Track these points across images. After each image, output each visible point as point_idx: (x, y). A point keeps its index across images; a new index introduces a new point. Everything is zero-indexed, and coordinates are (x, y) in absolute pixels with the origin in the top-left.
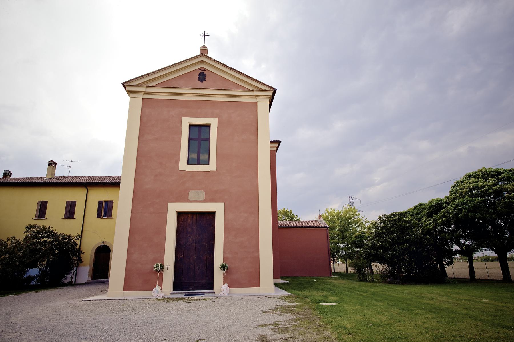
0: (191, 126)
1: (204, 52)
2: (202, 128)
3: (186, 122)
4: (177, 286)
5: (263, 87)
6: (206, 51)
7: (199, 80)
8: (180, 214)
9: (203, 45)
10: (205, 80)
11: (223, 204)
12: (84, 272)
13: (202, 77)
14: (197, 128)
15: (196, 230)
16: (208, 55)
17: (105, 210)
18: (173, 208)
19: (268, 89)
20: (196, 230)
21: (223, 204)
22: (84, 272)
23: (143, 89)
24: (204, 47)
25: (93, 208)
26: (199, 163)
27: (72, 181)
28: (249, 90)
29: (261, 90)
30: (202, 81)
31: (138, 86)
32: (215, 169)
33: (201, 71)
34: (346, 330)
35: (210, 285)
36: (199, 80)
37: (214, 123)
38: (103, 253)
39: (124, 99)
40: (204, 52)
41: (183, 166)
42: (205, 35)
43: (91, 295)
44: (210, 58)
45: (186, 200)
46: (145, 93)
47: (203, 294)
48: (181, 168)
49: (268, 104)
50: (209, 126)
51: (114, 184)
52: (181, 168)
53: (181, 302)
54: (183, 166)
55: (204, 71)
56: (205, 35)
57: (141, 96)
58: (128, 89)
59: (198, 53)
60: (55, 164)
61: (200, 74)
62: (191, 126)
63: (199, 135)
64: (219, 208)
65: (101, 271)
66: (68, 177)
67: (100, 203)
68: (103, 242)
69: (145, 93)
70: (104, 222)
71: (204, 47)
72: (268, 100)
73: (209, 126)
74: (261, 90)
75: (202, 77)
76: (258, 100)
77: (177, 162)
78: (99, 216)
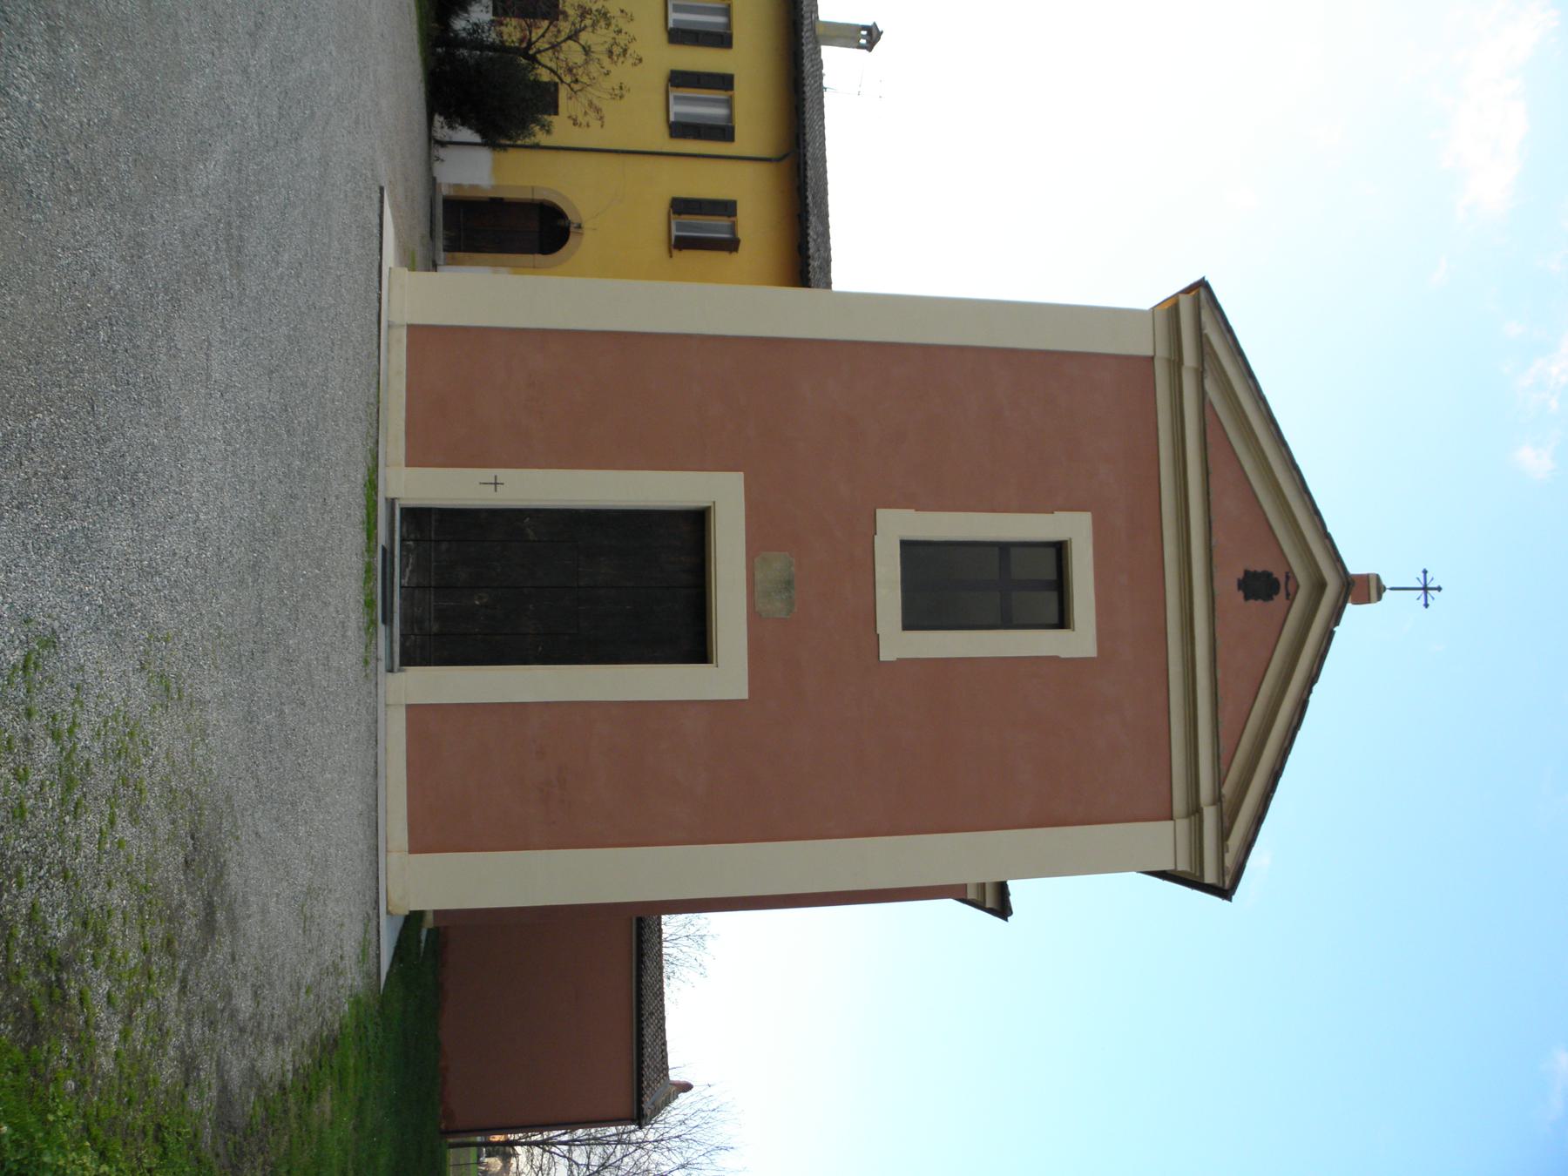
0: (1060, 550)
1: (1365, 589)
3: (1073, 528)
4: (421, 522)
5: (1235, 841)
6: (1365, 599)
7: (1247, 573)
8: (697, 521)
9: (1386, 582)
10: (1247, 598)
12: (474, 169)
13: (1259, 586)
14: (1051, 575)
15: (637, 587)
16: (1349, 606)
17: (699, 229)
18: (723, 495)
19: (1229, 860)
20: (637, 587)
22: (474, 169)
24: (1381, 590)
25: (706, 182)
26: (1060, 585)
27: (808, 105)
28: (1219, 781)
29: (1224, 834)
32: (888, 653)
33: (1282, 580)
35: (422, 648)
36: (1247, 573)
37: (1079, 640)
38: (537, 230)
39: (1143, 287)
40: (1365, 589)
41: (897, 525)
42: (1425, 589)
43: (394, 206)
44: (1336, 616)
45: (757, 543)
46: (1176, 363)
47: (387, 620)
48: (883, 515)
49: (1168, 866)
50: (1062, 621)
51: (802, 257)
52: (883, 515)
53: (361, 539)
54: (897, 525)
57: (1162, 352)
58: (1183, 298)
59: (1354, 567)
60: (870, 47)
61: (1267, 576)
62: (1060, 550)
63: (948, 585)
64: (725, 676)
65: (479, 228)
66: (820, 89)
67: (726, 208)
68: (579, 227)
69: (1176, 363)
70: (655, 223)
71: (1381, 590)
72: (1183, 866)
73: (1062, 621)
74: (1224, 834)
75: (1259, 586)
76: (1182, 825)
78: (681, 206)
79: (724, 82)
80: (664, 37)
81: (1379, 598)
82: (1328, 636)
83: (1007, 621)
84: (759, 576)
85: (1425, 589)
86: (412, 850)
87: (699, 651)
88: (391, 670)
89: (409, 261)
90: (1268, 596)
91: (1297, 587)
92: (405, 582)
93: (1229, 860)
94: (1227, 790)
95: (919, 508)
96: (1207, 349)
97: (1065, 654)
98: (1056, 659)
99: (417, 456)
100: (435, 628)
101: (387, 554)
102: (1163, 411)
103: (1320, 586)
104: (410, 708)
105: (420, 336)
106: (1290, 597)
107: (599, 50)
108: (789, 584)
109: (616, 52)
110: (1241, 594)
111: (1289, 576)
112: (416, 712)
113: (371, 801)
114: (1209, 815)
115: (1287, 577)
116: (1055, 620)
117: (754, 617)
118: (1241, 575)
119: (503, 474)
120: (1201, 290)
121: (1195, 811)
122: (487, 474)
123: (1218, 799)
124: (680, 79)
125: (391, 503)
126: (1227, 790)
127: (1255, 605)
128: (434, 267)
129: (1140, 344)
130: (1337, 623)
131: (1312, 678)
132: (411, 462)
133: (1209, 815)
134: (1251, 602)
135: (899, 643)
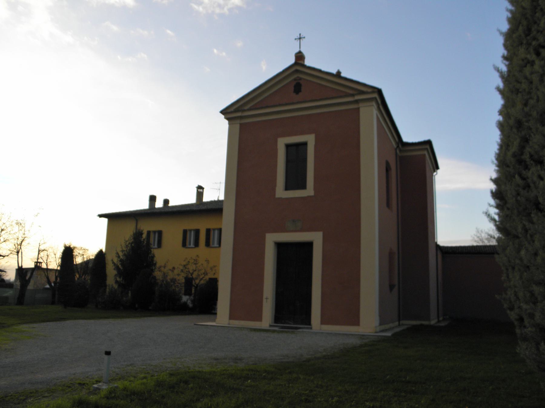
1: (300, 57)
3: (282, 143)
9: (297, 50)
13: (298, 88)
18: (271, 239)
19: (370, 90)
20: (294, 261)
24: (300, 52)
29: (363, 93)
31: (236, 111)
35: (307, 320)
37: (310, 139)
40: (300, 57)
41: (281, 192)
42: (300, 38)
46: (241, 118)
54: (281, 192)
57: (238, 121)
61: (295, 86)
64: (316, 238)
74: (363, 93)
75: (298, 88)
76: (361, 105)
79: (208, 231)
80: (197, 248)
85: (300, 38)
87: (309, 246)
88: (311, 328)
89: (214, 320)
91: (298, 77)
93: (370, 90)
95: (275, 186)
97: (314, 143)
99: (259, 318)
101: (282, 327)
102: (252, 120)
103: (297, 71)
105: (232, 317)
106: (301, 79)
107: (194, 267)
109: (196, 262)
111: (295, 80)
112: (323, 322)
114: (252, 104)
117: (302, 230)
119: (265, 297)
120: (223, 112)
121: (357, 102)
122: (264, 300)
123: (353, 95)
124: (208, 244)
125: (271, 326)
126: (351, 92)
127: (303, 89)
128: (216, 314)
129: (237, 127)
131: (320, 71)
133: (252, 104)
135: (309, 191)
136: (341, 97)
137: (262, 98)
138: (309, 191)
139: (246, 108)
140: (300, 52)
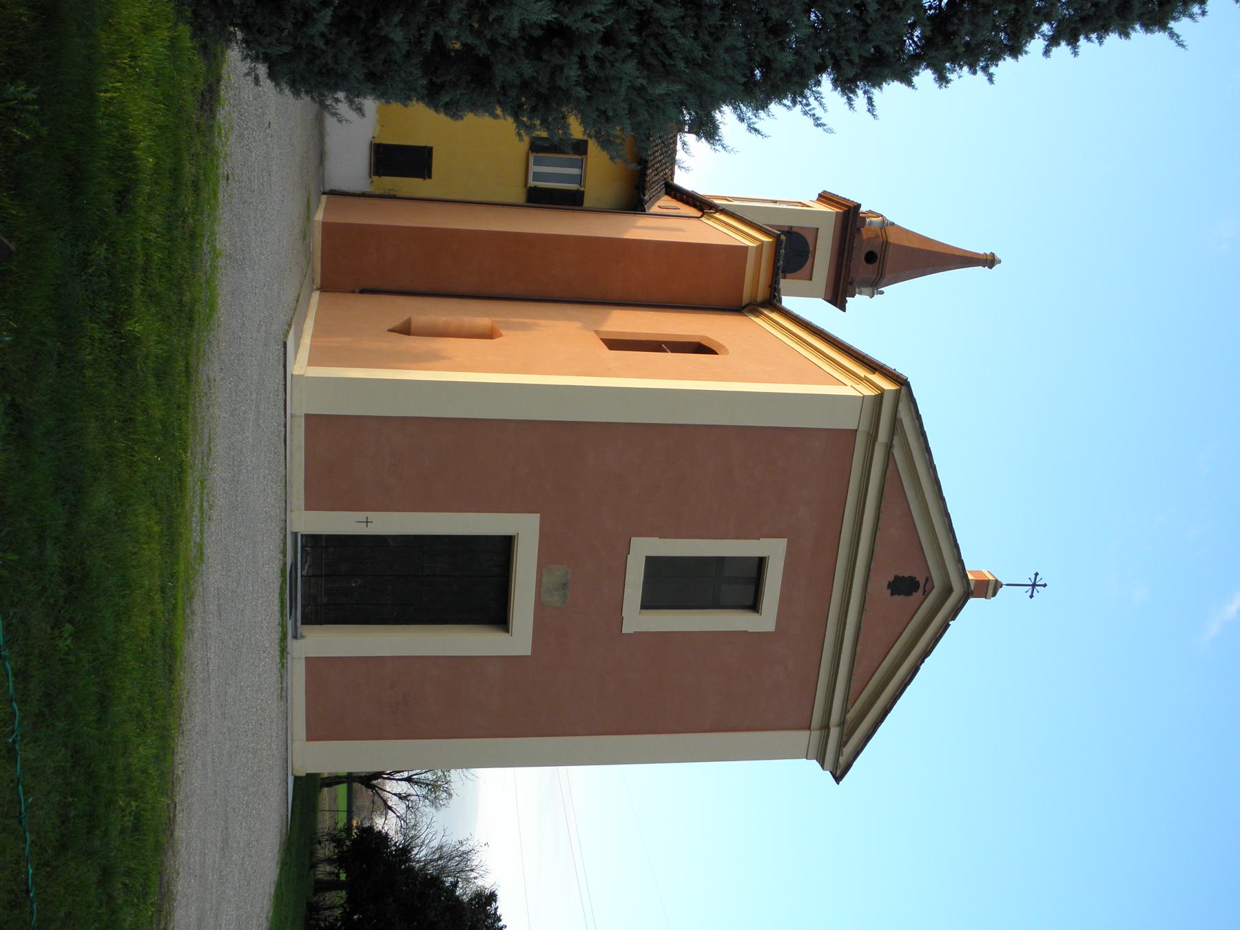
1: (987, 588)
2: (752, 588)
4: (315, 544)
5: (848, 749)
7: (896, 577)
8: (506, 544)
10: (892, 594)
11: (626, 630)
13: (904, 586)
14: (754, 574)
19: (842, 760)
20: (468, 582)
21: (626, 630)
23: (882, 437)
28: (845, 710)
29: (842, 744)
30: (922, 587)
31: (895, 421)
32: (636, 542)
34: (61, 602)
40: (987, 588)
41: (643, 548)
46: (872, 438)
48: (636, 542)
55: (921, 590)
56: (1034, 585)
57: (864, 428)
64: (518, 640)
69: (872, 438)
74: (842, 744)
75: (904, 586)
76: (816, 734)
77: (546, 536)
81: (994, 594)
82: (945, 627)
83: (716, 604)
84: (544, 581)
86: (307, 508)
87: (499, 618)
90: (909, 593)
92: (304, 573)
94: (850, 716)
96: (898, 425)
98: (746, 632)
99: (312, 504)
100: (325, 601)
101: (294, 565)
103: (948, 590)
104: (308, 659)
106: (926, 594)
108: (565, 585)
110: (889, 591)
111: (928, 579)
113: (283, 749)
114: (834, 732)
115: (927, 580)
116: (750, 603)
117: (539, 605)
118: (891, 579)
121: (825, 727)
122: (362, 515)
123: (842, 723)
125: (296, 534)
126: (850, 716)
127: (898, 599)
129: (847, 422)
130: (953, 619)
131: (927, 653)
132: (308, 507)
133: (834, 732)
134: (896, 597)
136: (846, 699)
137: (910, 493)
138: (637, 620)
139: (896, 442)
140: (997, 585)
